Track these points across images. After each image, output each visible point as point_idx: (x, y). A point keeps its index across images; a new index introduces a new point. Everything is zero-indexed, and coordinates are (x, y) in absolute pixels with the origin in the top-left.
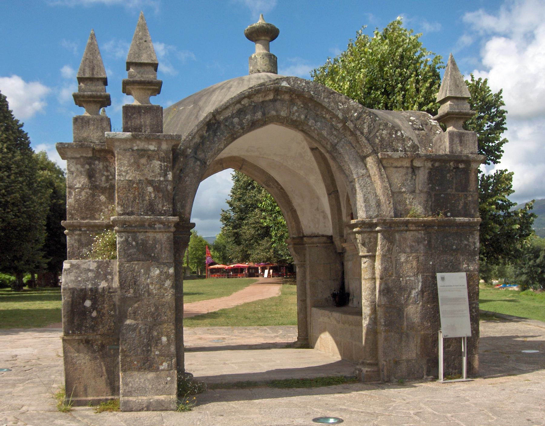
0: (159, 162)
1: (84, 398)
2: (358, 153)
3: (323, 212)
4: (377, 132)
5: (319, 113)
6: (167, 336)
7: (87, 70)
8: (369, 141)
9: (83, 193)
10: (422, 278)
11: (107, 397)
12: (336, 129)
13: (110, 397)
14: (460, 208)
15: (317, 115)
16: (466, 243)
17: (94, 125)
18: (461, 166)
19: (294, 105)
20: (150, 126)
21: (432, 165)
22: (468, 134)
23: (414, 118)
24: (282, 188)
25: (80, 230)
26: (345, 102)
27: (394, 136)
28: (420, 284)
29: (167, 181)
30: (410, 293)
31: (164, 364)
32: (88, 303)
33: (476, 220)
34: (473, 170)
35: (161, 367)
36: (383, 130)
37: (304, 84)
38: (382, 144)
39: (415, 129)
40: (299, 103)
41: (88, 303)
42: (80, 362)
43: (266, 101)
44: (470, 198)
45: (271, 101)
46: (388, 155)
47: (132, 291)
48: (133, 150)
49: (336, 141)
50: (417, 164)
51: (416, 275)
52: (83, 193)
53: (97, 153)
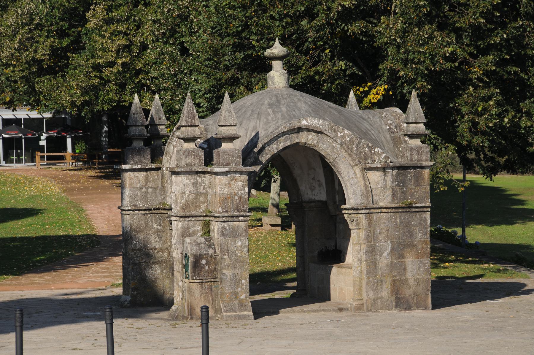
0: (241, 183)
3: (319, 181)
12: (336, 149)
26: (342, 131)
28: (390, 247)
32: (204, 262)
49: (335, 156)
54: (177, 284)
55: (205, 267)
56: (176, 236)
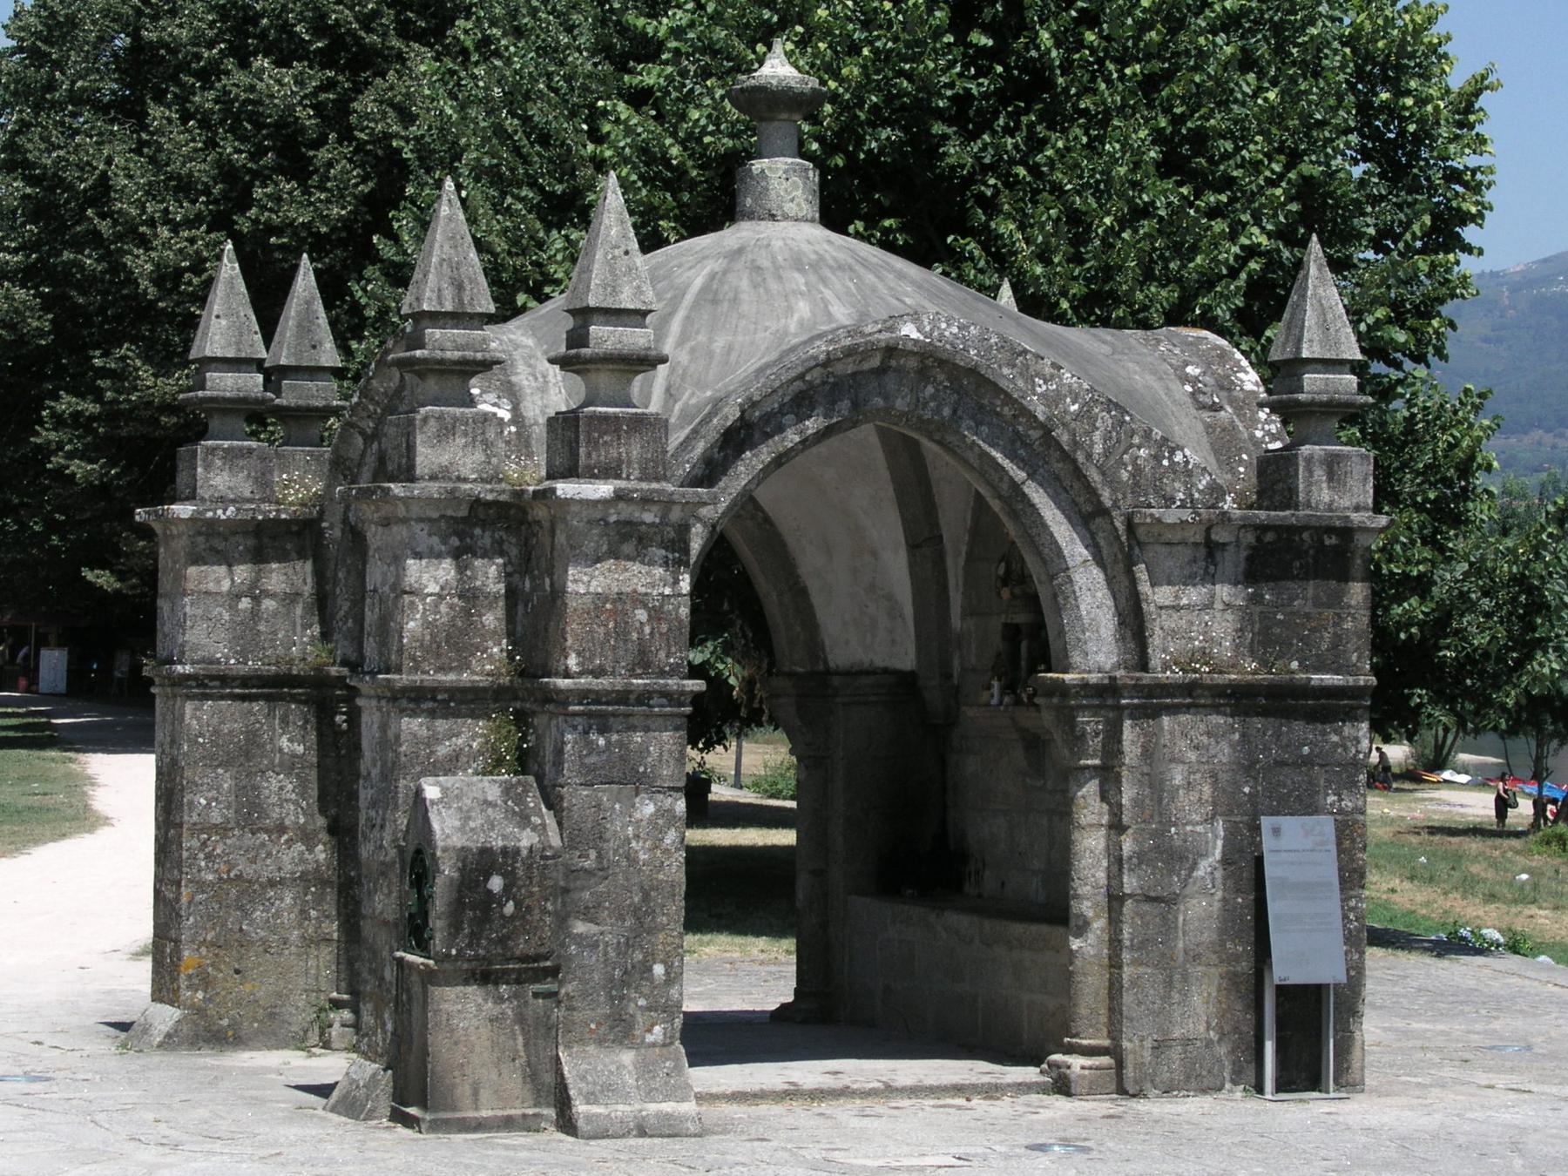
0: (663, 552)
1: (471, 1114)
2: (1076, 504)
3: (889, 597)
4: (1125, 452)
5: (986, 402)
6: (664, 962)
7: (448, 293)
8: (1104, 474)
9: (443, 608)
10: (1225, 830)
11: (513, 1112)
12: (1025, 445)
13: (531, 1111)
14: (1324, 647)
15: (981, 407)
16: (1335, 738)
17: (465, 434)
18: (1331, 541)
19: (927, 383)
20: (640, 463)
21: (1258, 539)
22: (1348, 457)
23: (1198, 371)
24: (767, 520)
25: (434, 699)
26: (1052, 377)
27: (1165, 463)
28: (1220, 843)
29: (680, 595)
30: (1194, 866)
31: (657, 1029)
32: (496, 883)
33: (1362, 680)
34: (1360, 552)
35: (649, 1038)
36: (1139, 448)
37: (955, 330)
38: (1136, 484)
39: (1203, 407)
40: (941, 377)
41: (496, 883)
42: (466, 1023)
43: (861, 372)
44: (1348, 625)
45: (873, 371)
46: (1152, 515)
47: (593, 854)
48: (607, 524)
50: (1220, 536)
51: (1210, 819)
52: (443, 608)
53: (481, 509)
54: (372, 972)
55: (501, 906)
56: (375, 772)
